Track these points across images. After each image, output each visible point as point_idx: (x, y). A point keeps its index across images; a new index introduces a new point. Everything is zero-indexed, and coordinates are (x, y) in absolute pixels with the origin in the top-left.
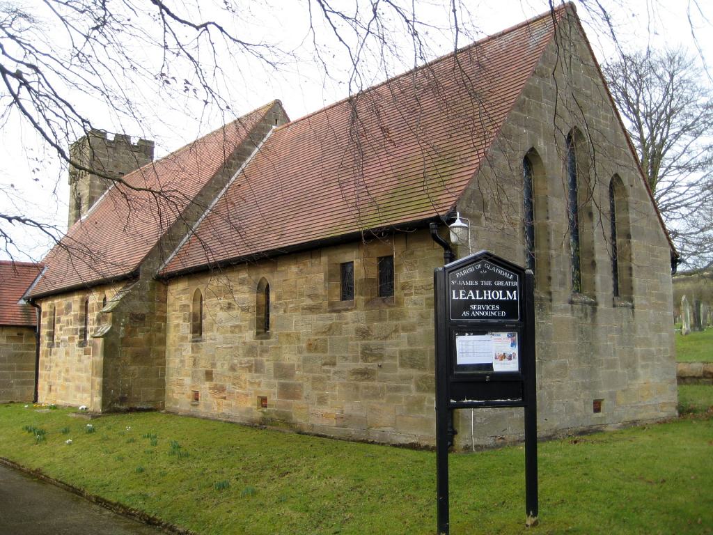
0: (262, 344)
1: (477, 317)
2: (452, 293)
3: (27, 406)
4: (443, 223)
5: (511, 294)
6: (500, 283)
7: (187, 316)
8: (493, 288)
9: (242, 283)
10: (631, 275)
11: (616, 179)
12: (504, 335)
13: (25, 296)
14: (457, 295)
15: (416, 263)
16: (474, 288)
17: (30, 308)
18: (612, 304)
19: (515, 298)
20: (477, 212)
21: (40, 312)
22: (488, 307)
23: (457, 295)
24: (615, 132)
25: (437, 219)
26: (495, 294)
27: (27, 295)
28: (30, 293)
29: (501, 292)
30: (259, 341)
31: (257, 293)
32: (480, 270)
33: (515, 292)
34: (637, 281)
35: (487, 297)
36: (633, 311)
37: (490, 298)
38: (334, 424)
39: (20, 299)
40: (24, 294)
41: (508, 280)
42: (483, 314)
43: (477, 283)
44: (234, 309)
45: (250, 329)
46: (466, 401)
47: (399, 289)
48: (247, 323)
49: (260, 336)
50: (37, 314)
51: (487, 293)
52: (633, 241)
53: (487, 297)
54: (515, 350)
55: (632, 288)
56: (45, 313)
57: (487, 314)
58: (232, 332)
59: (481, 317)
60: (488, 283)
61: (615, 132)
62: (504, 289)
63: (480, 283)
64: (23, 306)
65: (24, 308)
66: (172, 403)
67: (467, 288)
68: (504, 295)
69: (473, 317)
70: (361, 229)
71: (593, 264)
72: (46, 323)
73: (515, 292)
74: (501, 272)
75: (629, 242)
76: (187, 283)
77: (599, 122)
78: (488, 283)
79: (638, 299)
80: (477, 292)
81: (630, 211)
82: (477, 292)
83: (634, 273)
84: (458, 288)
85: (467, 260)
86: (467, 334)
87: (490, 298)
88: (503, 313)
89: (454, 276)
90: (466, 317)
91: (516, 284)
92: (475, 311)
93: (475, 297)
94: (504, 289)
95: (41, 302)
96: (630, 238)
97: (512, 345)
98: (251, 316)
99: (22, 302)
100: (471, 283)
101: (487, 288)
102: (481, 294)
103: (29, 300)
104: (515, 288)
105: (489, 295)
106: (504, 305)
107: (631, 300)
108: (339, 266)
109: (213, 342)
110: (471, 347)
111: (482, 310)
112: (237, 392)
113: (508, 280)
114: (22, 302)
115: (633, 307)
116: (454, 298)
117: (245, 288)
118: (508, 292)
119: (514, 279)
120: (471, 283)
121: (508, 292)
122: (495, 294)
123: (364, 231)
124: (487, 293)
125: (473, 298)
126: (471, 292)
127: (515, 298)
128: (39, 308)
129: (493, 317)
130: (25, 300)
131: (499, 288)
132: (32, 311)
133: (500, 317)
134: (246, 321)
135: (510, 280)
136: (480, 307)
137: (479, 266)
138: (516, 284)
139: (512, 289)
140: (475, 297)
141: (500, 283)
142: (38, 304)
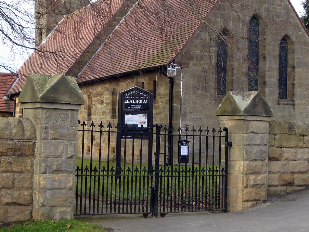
0: (113, 121)
1: (133, 109)
2: (124, 101)
3: (57, 231)
4: (165, 68)
5: (146, 101)
6: (141, 98)
7: (86, 107)
8: (139, 99)
9: (107, 90)
10: (294, 88)
11: (285, 39)
12: (142, 115)
13: (7, 94)
14: (126, 101)
15: (163, 84)
16: (132, 99)
17: (10, 101)
18: (277, 103)
19: (147, 103)
20: (187, 61)
21: (15, 104)
22: (137, 106)
23: (126, 101)
24: (288, 12)
25: (163, 66)
26: (140, 101)
27: (8, 93)
28: (11, 91)
29: (142, 101)
30: (112, 120)
31: (112, 95)
32: (135, 93)
33: (147, 101)
34: (297, 91)
35: (137, 102)
36: (294, 107)
37: (138, 103)
38: (137, 159)
39: (4, 96)
40: (6, 92)
41: (145, 96)
42: (135, 108)
43: (133, 97)
44: (104, 103)
45: (110, 114)
46: (128, 137)
47: (158, 95)
48: (108, 110)
49: (113, 117)
50: (14, 105)
51: (137, 101)
52: (297, 70)
53: (137, 102)
54: (146, 120)
55: (294, 95)
56: (18, 104)
57: (136, 108)
58: (103, 115)
59: (134, 109)
60: (137, 97)
61: (288, 12)
62: (143, 100)
63: (134, 98)
64: (6, 100)
65: (6, 101)
66: (79, 154)
67: (130, 99)
68: (143, 101)
69: (132, 109)
70: (130, 70)
71: (265, 83)
72: (19, 110)
73: (147, 101)
74: (142, 94)
75: (294, 70)
76: (101, 86)
77: (275, 8)
78: (137, 97)
79: (297, 101)
80: (133, 100)
81: (295, 54)
82: (133, 100)
83: (296, 87)
84: (126, 99)
85: (128, 91)
86: (129, 115)
87: (138, 103)
88: (142, 108)
89: (125, 96)
90: (129, 109)
91: (147, 98)
92: (132, 107)
93: (133, 102)
94: (143, 100)
95: (16, 97)
96: (295, 68)
97: (145, 119)
98: (110, 107)
99: (5, 98)
100: (131, 97)
101: (137, 99)
102: (135, 101)
103: (9, 96)
104: (147, 99)
105: (137, 102)
106: (143, 105)
107: (293, 101)
108: (141, 83)
109: (96, 120)
110: (130, 119)
111: (135, 107)
112: (104, 146)
113: (145, 96)
114: (5, 98)
115: (294, 105)
116: (125, 102)
117: (108, 92)
118: (144, 101)
119: (147, 96)
120: (131, 97)
121: (144, 101)
122: (140, 101)
123: (131, 71)
124: (137, 101)
125: (132, 102)
126: (131, 100)
127: (147, 103)
128: (15, 101)
129: (139, 109)
130: (6, 96)
131: (141, 99)
132: (11, 103)
133: (141, 109)
134: (108, 109)
135: (146, 97)
136: (134, 106)
137: (134, 92)
138: (147, 98)
139: (146, 100)
140: (133, 102)
141: (141, 98)
142: (14, 99)
